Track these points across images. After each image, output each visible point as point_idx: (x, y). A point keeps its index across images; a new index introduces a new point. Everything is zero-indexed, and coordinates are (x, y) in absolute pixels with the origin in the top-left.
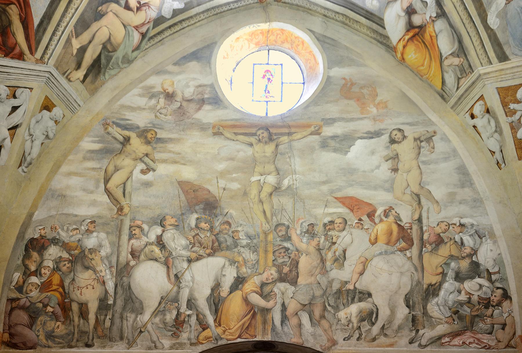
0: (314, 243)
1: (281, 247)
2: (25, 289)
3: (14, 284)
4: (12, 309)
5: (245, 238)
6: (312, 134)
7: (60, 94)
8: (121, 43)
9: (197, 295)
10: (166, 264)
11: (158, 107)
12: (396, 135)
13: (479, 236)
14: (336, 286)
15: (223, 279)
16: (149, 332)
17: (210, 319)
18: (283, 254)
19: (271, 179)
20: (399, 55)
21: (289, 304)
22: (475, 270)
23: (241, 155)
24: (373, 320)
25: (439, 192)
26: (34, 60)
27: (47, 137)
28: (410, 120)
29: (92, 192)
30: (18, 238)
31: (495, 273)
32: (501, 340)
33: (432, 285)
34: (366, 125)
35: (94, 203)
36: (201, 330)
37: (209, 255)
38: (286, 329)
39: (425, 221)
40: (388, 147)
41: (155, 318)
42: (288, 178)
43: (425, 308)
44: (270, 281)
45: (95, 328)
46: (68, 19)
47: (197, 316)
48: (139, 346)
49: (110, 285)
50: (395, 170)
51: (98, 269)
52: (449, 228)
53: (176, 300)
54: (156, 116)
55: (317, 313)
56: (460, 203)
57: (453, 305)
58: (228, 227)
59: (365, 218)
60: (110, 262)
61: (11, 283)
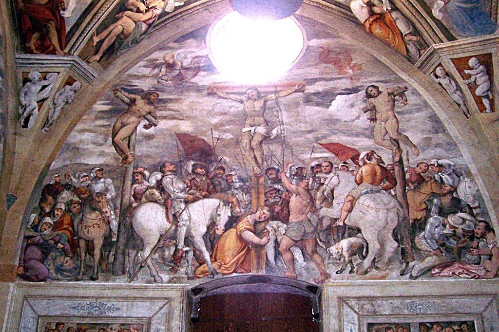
0: (303, 184)
1: (272, 188)
2: (39, 228)
3: (30, 224)
4: (28, 245)
5: (238, 181)
6: (296, 91)
7: (81, 73)
8: (130, 33)
9: (193, 233)
10: (165, 205)
11: (161, 75)
12: (371, 91)
13: (457, 175)
14: (326, 223)
15: (218, 218)
16: (148, 266)
17: (207, 256)
18: (274, 195)
19: (261, 130)
20: (368, 30)
21: (281, 240)
22: (457, 205)
23: (233, 109)
24: (364, 253)
25: (415, 138)
26: (63, 53)
27: (67, 103)
28: (383, 79)
29: (101, 145)
30: (37, 184)
31: (475, 208)
32: (489, 270)
33: (418, 220)
34: (344, 84)
35: (102, 154)
36: (198, 264)
37: (205, 197)
38: (279, 264)
39: (405, 163)
40: (365, 101)
41: (155, 254)
42: (277, 128)
43: (412, 241)
44: (263, 219)
45: (100, 263)
46: (92, 25)
47: (194, 252)
48: (140, 280)
49: (114, 224)
50: (374, 120)
51: (104, 210)
52: (428, 168)
53: (174, 237)
54: (158, 82)
55: (309, 248)
56: (436, 147)
57: (439, 238)
58: (222, 172)
59: (349, 161)
60: (115, 205)
61: (28, 222)
